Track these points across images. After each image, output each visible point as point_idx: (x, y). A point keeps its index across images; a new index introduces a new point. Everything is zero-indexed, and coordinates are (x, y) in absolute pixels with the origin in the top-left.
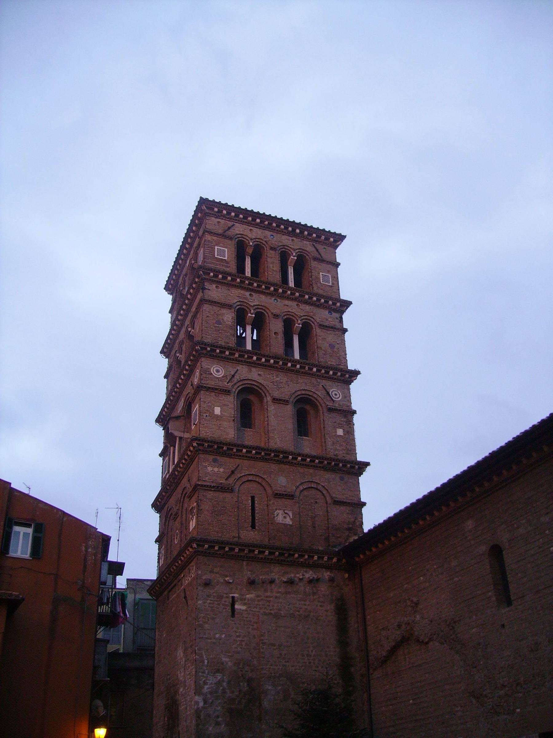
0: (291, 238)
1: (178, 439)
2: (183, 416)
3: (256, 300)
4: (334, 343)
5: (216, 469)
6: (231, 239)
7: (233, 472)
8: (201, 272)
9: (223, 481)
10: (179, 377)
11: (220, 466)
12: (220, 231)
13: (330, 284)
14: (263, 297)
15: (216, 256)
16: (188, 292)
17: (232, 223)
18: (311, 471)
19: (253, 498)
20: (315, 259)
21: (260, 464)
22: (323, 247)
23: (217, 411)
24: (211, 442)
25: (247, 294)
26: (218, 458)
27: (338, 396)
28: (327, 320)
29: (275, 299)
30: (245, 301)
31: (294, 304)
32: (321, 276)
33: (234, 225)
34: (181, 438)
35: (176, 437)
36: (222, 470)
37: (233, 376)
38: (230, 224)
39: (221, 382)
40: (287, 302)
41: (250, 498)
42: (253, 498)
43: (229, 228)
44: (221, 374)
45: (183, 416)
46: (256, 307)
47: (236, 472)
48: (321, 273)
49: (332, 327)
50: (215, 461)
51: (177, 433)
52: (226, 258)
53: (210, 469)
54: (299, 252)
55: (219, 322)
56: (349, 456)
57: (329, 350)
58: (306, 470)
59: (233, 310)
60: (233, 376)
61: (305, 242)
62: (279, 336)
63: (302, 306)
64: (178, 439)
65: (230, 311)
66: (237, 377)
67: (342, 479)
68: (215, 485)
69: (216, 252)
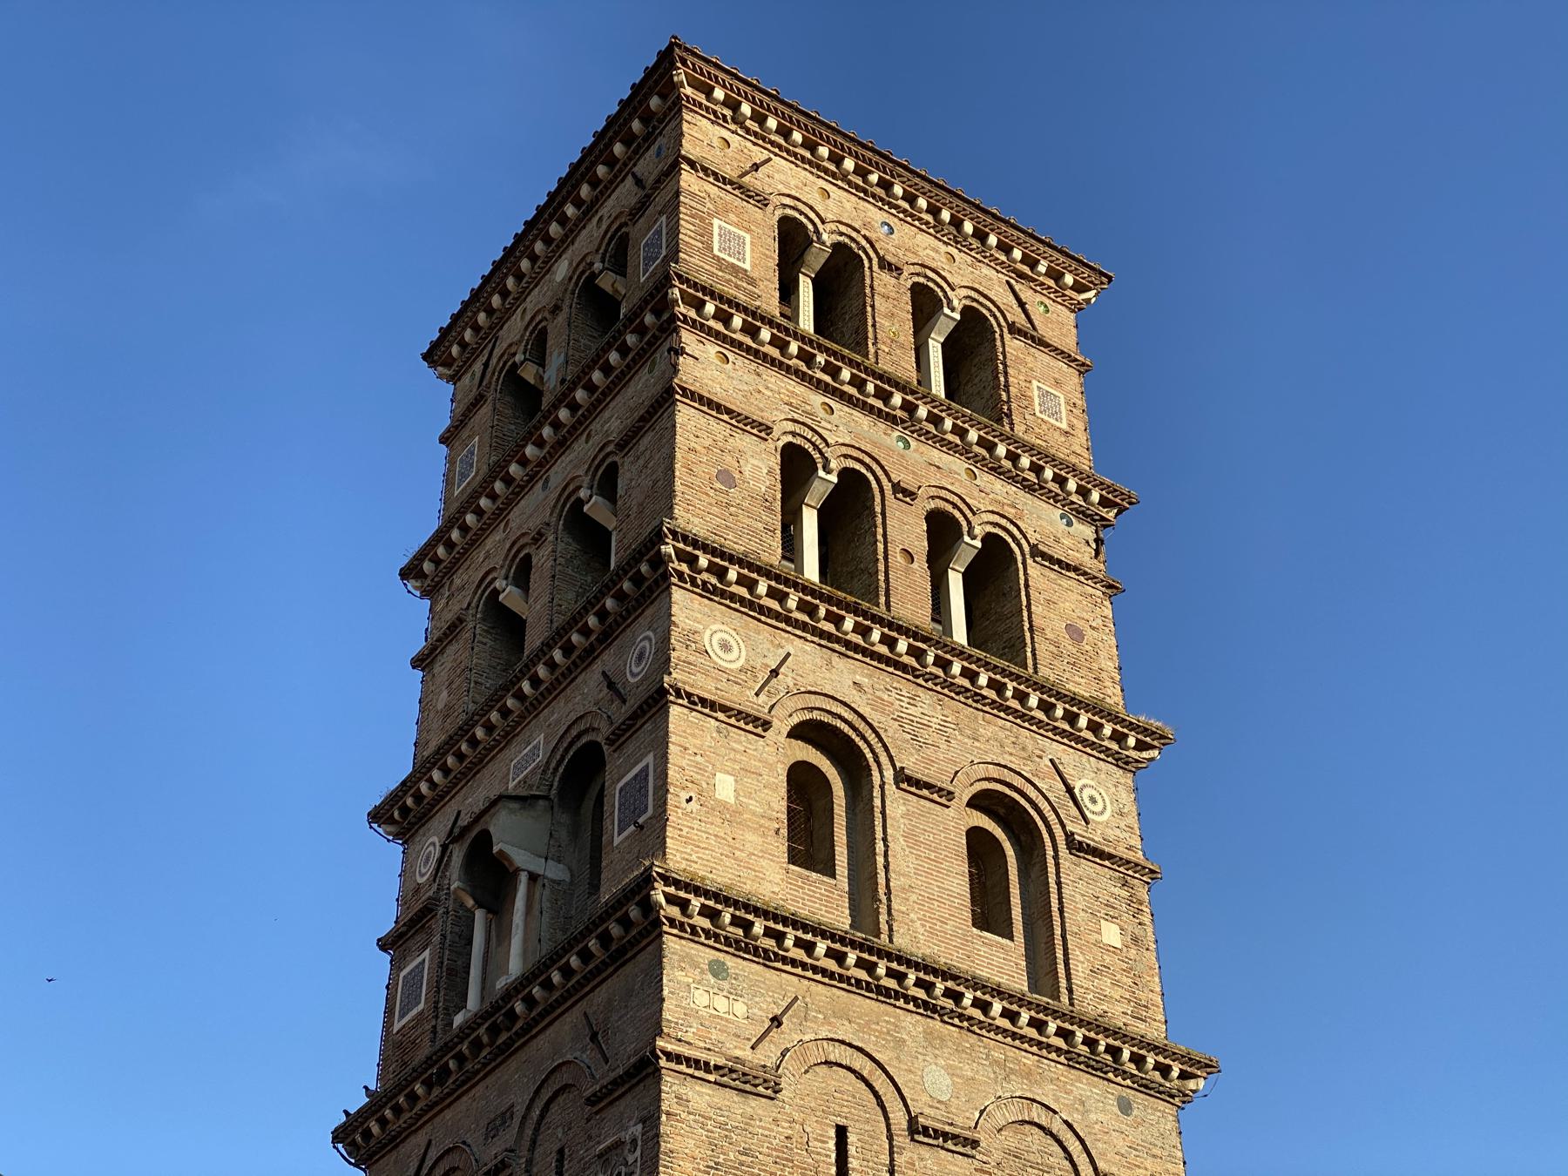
0: (943, 248)
1: (523, 877)
2: (546, 798)
3: (846, 432)
4: (1080, 624)
5: (721, 1004)
6: (763, 203)
7: (776, 1021)
8: (676, 291)
9: (745, 1053)
10: (510, 686)
11: (734, 995)
12: (730, 172)
13: (1064, 426)
14: (863, 421)
15: (716, 252)
16: (565, 399)
17: (766, 154)
18: (1029, 1060)
19: (841, 1132)
20: (1014, 329)
21: (864, 1005)
22: (1039, 298)
23: (725, 788)
24: (716, 896)
25: (817, 399)
26: (730, 962)
27: (1098, 808)
28: (1057, 541)
29: (900, 438)
30: (809, 422)
31: (958, 464)
32: (1036, 393)
33: (769, 160)
34: (533, 877)
35: (518, 870)
36: (740, 1008)
37: (775, 673)
38: (759, 155)
39: (736, 687)
40: (937, 455)
41: (832, 1133)
42: (841, 1132)
43: (756, 167)
44: (735, 660)
45: (546, 798)
46: (853, 450)
47: (767, 1024)
48: (1035, 383)
49: (1076, 569)
50: (718, 970)
51: (521, 858)
52: (747, 266)
53: (701, 998)
54: (967, 297)
55: (726, 478)
56: (1142, 1026)
57: (1068, 646)
58: (1012, 1053)
59: (771, 445)
60: (775, 673)
61: (986, 271)
62: (915, 565)
63: (985, 479)
64: (523, 877)
65: (763, 445)
66: (786, 679)
67: (1125, 1107)
68: (721, 1061)
69: (716, 238)
